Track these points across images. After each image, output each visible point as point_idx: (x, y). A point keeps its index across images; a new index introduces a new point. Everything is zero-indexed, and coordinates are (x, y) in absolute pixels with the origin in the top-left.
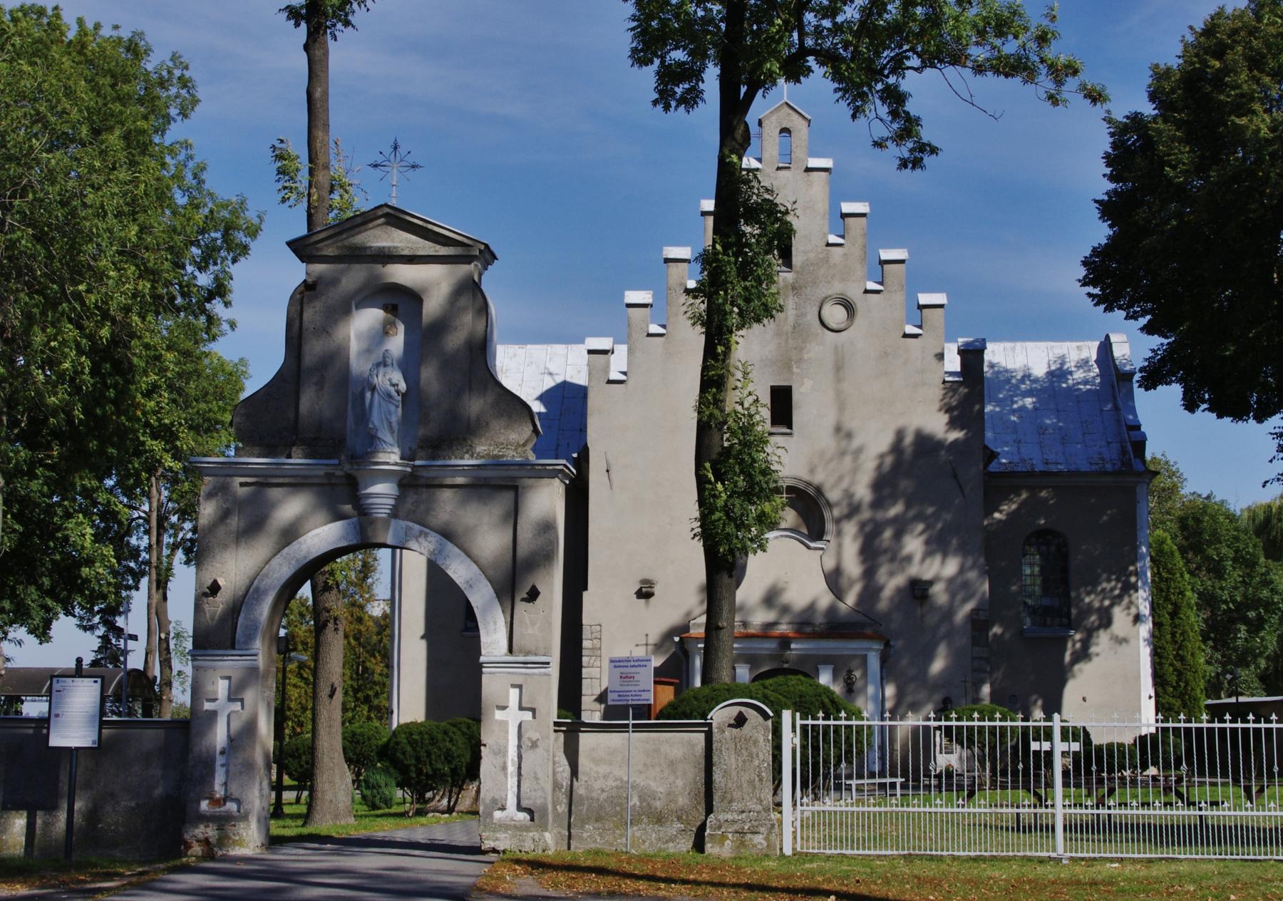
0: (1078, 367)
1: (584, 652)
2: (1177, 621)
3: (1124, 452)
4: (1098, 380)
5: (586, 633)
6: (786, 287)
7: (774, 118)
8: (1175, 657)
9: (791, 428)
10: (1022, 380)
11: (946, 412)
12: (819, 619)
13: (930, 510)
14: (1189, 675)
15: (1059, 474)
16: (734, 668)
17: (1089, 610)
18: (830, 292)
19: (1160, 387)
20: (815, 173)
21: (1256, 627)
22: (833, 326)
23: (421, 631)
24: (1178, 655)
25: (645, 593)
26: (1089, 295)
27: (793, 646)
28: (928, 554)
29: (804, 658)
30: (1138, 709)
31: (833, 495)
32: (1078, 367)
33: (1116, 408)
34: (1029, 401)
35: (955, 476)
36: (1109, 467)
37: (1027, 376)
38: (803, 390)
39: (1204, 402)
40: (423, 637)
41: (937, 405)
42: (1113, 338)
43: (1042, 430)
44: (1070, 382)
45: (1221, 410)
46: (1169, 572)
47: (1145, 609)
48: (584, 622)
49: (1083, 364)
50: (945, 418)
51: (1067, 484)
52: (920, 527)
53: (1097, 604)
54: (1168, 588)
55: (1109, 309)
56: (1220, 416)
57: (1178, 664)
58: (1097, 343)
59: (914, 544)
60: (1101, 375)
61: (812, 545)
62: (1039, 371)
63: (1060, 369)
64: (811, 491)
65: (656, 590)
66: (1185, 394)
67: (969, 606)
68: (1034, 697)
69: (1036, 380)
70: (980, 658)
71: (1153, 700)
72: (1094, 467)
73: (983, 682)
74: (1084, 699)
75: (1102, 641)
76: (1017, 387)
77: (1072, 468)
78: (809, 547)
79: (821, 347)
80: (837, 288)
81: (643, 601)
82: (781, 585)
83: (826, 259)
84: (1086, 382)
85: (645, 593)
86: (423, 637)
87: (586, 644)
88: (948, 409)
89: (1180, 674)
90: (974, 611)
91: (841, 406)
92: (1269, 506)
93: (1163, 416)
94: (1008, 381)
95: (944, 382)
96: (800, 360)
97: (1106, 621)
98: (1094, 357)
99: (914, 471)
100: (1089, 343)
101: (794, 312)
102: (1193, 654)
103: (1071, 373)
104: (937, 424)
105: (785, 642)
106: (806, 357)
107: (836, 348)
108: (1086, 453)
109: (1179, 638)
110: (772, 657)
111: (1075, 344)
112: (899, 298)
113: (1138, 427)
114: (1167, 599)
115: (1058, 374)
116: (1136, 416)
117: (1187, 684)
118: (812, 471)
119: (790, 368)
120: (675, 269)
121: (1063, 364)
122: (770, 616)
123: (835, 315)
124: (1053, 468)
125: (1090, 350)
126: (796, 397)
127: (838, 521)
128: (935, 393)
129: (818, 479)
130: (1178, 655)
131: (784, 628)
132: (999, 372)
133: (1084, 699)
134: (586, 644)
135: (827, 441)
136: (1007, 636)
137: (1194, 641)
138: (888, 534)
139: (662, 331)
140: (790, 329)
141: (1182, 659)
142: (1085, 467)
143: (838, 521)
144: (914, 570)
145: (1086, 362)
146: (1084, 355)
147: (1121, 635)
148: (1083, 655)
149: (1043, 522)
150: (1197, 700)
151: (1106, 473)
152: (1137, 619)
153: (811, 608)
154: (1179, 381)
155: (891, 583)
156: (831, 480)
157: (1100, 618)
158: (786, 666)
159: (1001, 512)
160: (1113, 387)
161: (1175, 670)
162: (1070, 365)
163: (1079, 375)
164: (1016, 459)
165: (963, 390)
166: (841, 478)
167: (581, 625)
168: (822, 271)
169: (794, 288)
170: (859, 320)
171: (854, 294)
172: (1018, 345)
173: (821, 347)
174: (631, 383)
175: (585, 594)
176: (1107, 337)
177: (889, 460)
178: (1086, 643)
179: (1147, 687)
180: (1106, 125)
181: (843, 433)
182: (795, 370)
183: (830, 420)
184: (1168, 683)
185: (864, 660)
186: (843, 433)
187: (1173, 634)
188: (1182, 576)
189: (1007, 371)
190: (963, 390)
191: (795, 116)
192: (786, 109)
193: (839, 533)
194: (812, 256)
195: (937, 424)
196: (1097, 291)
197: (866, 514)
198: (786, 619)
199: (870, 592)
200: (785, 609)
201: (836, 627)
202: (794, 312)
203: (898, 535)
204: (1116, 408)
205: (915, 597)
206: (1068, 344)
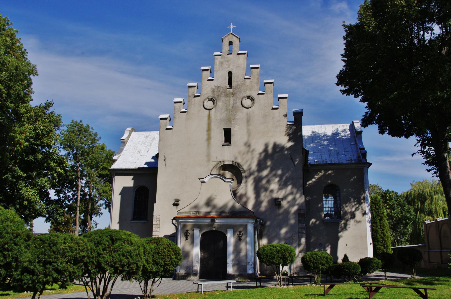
0: (343, 132)
1: (154, 226)
2: (382, 222)
3: (359, 157)
4: (350, 135)
5: (155, 219)
6: (230, 94)
7: (227, 38)
8: (381, 233)
9: (230, 143)
10: (323, 136)
11: (288, 136)
12: (227, 210)
13: (279, 172)
14: (386, 239)
15: (335, 164)
16: (193, 230)
17: (346, 213)
18: (245, 95)
19: (369, 126)
20: (241, 55)
21: (405, 225)
22: (246, 106)
23: (118, 221)
24: (382, 232)
25: (176, 204)
26: (340, 90)
27: (217, 221)
28: (280, 189)
29: (221, 226)
30: (366, 248)
31: (245, 167)
32: (343, 132)
33: (356, 144)
34: (325, 143)
35: (292, 159)
36: (353, 162)
37: (325, 135)
38: (235, 129)
39: (387, 130)
41: (284, 133)
42: (354, 122)
43: (330, 151)
44: (340, 136)
45: (394, 133)
46: (379, 207)
47: (367, 210)
48: (154, 215)
49: (345, 130)
50: (287, 138)
51: (338, 168)
52: (277, 179)
53: (350, 210)
54: (378, 212)
55: (348, 95)
56: (393, 136)
57: (382, 235)
58: (349, 124)
59: (274, 186)
60: (351, 134)
61: (226, 180)
62: (329, 133)
63: (336, 133)
64: (236, 165)
65: (179, 203)
66: (379, 127)
67: (295, 208)
68: (328, 244)
69: (328, 136)
70: (301, 228)
71: (372, 245)
72: (348, 162)
73: (302, 237)
74: (346, 245)
75: (352, 222)
76: (321, 138)
77: (340, 162)
78: (225, 181)
79: (242, 114)
80: (248, 93)
81: (175, 207)
82: (214, 196)
83: (244, 84)
84: (345, 136)
85: (176, 204)
87: (154, 223)
88: (289, 135)
89: (383, 238)
90: (298, 210)
91: (249, 135)
92: (407, 192)
93: (372, 136)
94: (319, 137)
95: (287, 125)
97: (353, 216)
98: (348, 128)
99: (273, 157)
100: (347, 124)
101: (232, 102)
102: (387, 232)
103: (340, 134)
104: (285, 141)
105: (213, 220)
106: (236, 117)
107: (247, 114)
108: (346, 157)
109: (382, 227)
110: (208, 226)
111: (342, 125)
112: (271, 96)
113: (364, 149)
114: (378, 215)
115: (336, 134)
116: (362, 145)
117: (385, 241)
118: (236, 158)
119: (231, 122)
120: (191, 90)
121: (337, 131)
122: (208, 210)
123: (247, 103)
124: (333, 162)
125: (347, 126)
126: (232, 132)
127: (246, 177)
128: (284, 128)
129: (239, 161)
130: (382, 232)
131: (213, 214)
132: (315, 134)
133: (346, 245)
134: (154, 223)
135: (243, 148)
136: (318, 222)
137: (387, 228)
138: (264, 182)
139: (186, 111)
140: (231, 108)
141: (383, 234)
142: (345, 162)
143: (246, 177)
144: (275, 195)
145: (345, 130)
146: (345, 128)
147: (358, 220)
148: (345, 228)
149: (330, 182)
150: (388, 246)
151: (353, 164)
152: (364, 214)
153: (225, 206)
154: (376, 123)
155: (265, 198)
156: (244, 162)
157: (351, 215)
158: (214, 229)
159: (315, 178)
160: (355, 137)
161: (381, 237)
162: (340, 131)
163: (343, 134)
164: (321, 160)
165: (294, 127)
166: (247, 161)
167: (153, 216)
168: (242, 88)
169: (232, 94)
170: (256, 104)
171: (254, 94)
172: (323, 126)
173: (242, 114)
174: (174, 129)
175: (155, 204)
176: (353, 122)
177: (263, 155)
178: (346, 225)
179: (370, 240)
180: (343, 28)
181: (248, 145)
182: (232, 122)
183: (245, 139)
184: (379, 241)
185: (246, 227)
186: (248, 145)
187: (380, 226)
188: (383, 208)
189: (319, 134)
190: (294, 127)
191: (234, 37)
192: (231, 35)
193: (246, 182)
194: (239, 83)
195: (285, 141)
196: (343, 88)
197: (256, 174)
198: (214, 210)
199: (258, 203)
200: (214, 207)
201: (234, 213)
202: (232, 102)
203: (268, 182)
204: (356, 144)
205: (276, 205)
206: (340, 125)
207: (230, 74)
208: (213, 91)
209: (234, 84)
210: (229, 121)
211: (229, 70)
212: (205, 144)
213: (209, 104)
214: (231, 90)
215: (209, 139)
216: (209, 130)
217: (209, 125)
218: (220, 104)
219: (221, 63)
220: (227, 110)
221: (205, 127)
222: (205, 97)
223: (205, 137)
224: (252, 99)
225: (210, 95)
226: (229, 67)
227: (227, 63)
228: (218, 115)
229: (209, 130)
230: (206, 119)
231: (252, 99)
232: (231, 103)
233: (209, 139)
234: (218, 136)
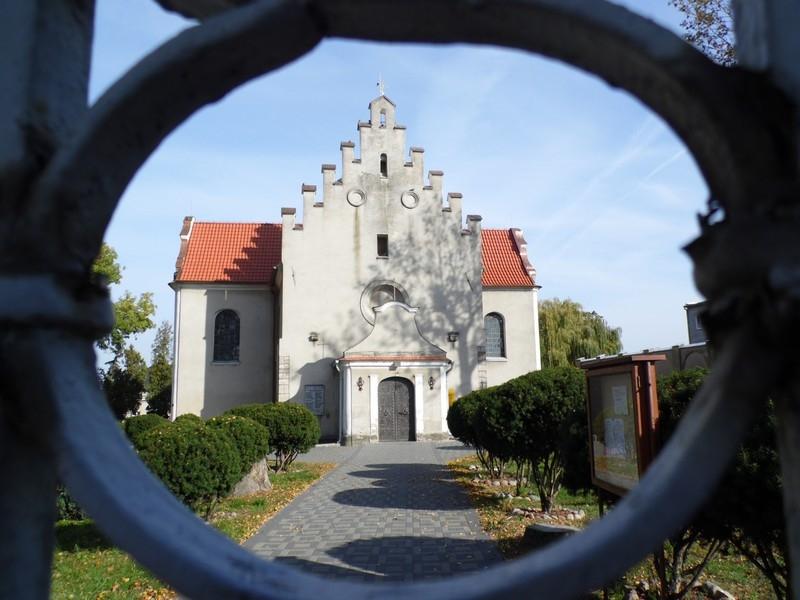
32: (454, 272)
40: (205, 338)
83: (404, 173)
86: (205, 338)
87: (281, 366)
96: (392, 223)
123: (409, 200)
169: (388, 186)
171: (418, 190)
191: (388, 104)
194: (397, 171)
207: (384, 156)
208: (361, 179)
209: (390, 172)
210: (385, 223)
211: (382, 151)
212: (352, 255)
213: (355, 198)
214: (386, 180)
215: (357, 248)
216: (357, 235)
217: (357, 227)
218: (371, 199)
219: (371, 140)
220: (381, 209)
221: (351, 231)
222: (349, 188)
223: (352, 244)
224: (416, 198)
225: (357, 185)
226: (382, 147)
227: (379, 141)
228: (370, 215)
229: (357, 235)
230: (352, 220)
231: (416, 198)
232: (387, 199)
233: (357, 248)
234: (372, 246)
